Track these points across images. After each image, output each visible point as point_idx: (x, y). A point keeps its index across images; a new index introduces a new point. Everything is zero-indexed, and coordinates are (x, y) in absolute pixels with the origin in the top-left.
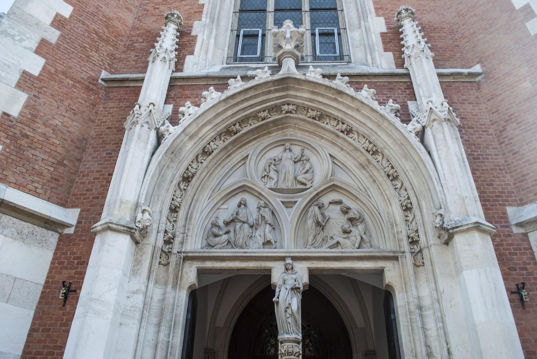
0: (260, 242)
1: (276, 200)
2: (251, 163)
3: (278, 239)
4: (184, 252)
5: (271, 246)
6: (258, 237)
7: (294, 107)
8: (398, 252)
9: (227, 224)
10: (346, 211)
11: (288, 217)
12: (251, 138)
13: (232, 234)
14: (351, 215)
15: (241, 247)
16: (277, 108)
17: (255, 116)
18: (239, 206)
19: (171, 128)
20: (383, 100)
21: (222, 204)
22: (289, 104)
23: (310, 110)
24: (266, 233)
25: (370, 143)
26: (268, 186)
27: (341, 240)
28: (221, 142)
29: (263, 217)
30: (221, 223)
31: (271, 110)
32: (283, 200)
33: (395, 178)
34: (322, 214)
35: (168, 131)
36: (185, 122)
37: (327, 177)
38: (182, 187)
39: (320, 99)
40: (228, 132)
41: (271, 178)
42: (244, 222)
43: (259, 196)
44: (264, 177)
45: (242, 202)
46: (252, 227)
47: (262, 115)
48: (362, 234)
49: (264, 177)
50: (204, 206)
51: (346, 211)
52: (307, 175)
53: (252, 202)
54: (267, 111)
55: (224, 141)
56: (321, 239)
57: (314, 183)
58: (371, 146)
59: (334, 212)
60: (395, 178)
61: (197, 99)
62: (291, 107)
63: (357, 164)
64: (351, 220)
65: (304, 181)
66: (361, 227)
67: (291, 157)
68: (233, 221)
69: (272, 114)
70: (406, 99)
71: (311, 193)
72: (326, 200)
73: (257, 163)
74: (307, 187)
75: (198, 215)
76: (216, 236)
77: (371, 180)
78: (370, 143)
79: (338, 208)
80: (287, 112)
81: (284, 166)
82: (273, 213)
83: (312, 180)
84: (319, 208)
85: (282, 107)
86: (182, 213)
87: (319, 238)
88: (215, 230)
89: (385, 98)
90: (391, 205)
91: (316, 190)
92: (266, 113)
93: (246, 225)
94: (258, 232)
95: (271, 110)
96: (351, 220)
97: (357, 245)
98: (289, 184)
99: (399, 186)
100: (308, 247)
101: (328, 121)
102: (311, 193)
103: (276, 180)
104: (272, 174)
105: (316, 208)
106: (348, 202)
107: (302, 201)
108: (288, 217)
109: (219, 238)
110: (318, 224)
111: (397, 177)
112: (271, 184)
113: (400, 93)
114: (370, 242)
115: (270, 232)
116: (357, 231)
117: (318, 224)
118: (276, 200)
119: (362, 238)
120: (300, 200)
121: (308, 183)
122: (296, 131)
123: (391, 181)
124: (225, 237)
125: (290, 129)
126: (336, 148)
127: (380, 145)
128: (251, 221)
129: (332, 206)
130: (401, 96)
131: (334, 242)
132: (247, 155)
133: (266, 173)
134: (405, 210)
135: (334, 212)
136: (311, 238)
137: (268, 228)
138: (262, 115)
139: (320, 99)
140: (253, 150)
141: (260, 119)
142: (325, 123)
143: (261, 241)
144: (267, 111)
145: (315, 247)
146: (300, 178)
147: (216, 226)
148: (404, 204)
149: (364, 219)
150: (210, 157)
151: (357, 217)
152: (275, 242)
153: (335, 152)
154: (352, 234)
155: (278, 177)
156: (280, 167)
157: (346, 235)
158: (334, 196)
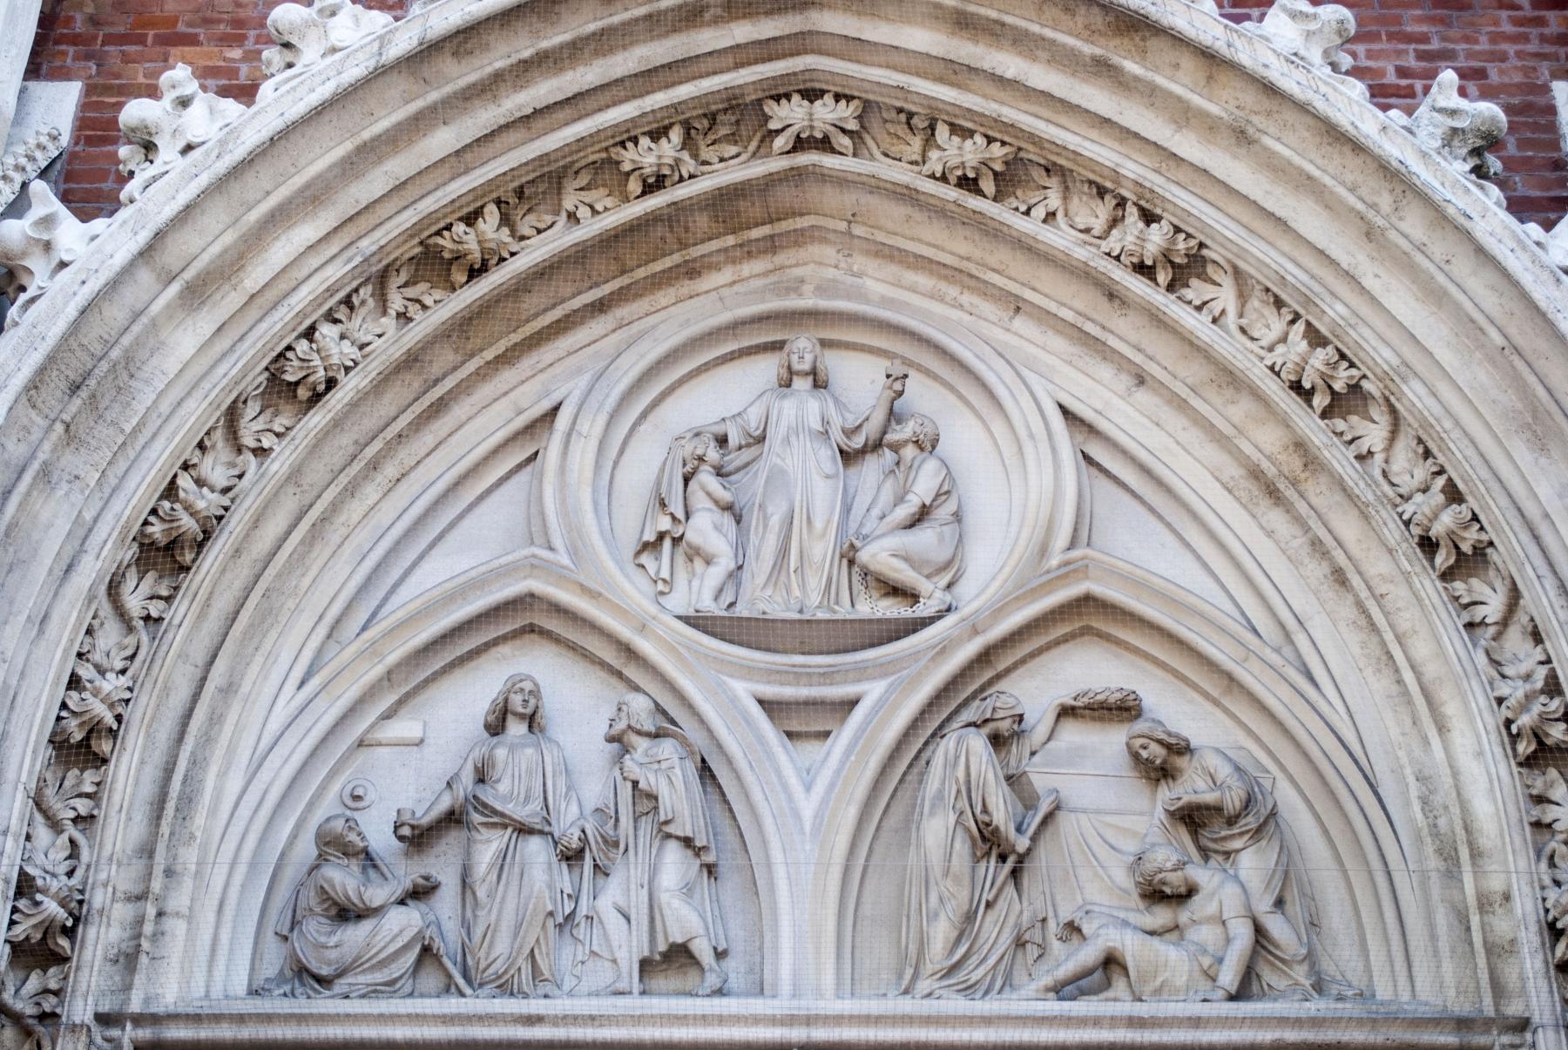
0: (621, 955)
1: (726, 694)
2: (572, 457)
3: (737, 935)
4: (138, 1020)
5: (692, 979)
6: (614, 921)
7: (847, 113)
8: (1488, 1024)
9: (418, 838)
10: (1160, 763)
11: (802, 800)
12: (577, 303)
13: (446, 903)
14: (1192, 787)
15: (506, 988)
16: (738, 117)
17: (602, 166)
18: (496, 727)
19: (71, 233)
20: (1402, 72)
21: (388, 715)
22: (812, 95)
23: (942, 132)
24: (663, 897)
25: (1316, 338)
26: (679, 601)
27: (1131, 946)
28: (389, 323)
29: (645, 798)
30: (378, 834)
31: (701, 125)
32: (771, 691)
33: (1471, 561)
34: (1014, 780)
35: (47, 246)
36: (156, 190)
37: (1043, 551)
38: (134, 603)
39: (1009, 64)
40: (433, 262)
41: (694, 553)
42: (524, 830)
43: (622, 662)
44: (652, 546)
45: (516, 701)
46: (572, 857)
47: (647, 156)
48: (1263, 905)
49: (652, 546)
50: (274, 725)
51: (1160, 763)
52: (925, 539)
53: (578, 703)
54: (676, 135)
55: (403, 317)
56: (1007, 939)
57: (966, 589)
58: (1320, 357)
59: (1087, 775)
60: (1471, 561)
61: (236, 53)
62: (826, 113)
63: (1233, 471)
64: (1192, 818)
65: (904, 574)
66: (1253, 863)
67: (825, 422)
68: (453, 819)
69: (705, 153)
70: (1544, 69)
71: (943, 649)
72: (1035, 691)
73: (609, 458)
74: (923, 610)
75: (234, 785)
76: (345, 913)
77: (1317, 570)
78: (1316, 338)
79: (1111, 741)
80: (800, 144)
81: (778, 477)
82: (705, 770)
83: (950, 569)
84: (997, 741)
85: (770, 107)
86: (130, 772)
87: (995, 932)
88: (343, 879)
89: (1411, 62)
90: (1442, 728)
91: (975, 631)
92: (669, 148)
93: (535, 845)
94: (612, 893)
95: (701, 125)
96: (1192, 818)
97: (1229, 977)
98: (811, 592)
99: (1493, 609)
100: (923, 986)
101: (1054, 201)
102: (943, 649)
103: (725, 563)
104: (706, 528)
105: (978, 743)
106: (1172, 708)
107: (887, 694)
108: (802, 800)
109: (366, 926)
110: (988, 841)
111: (1480, 553)
112: (699, 590)
113: (1508, 28)
114: (1310, 958)
115: (688, 890)
116: (1231, 889)
117: (988, 841)
118: (726, 694)
119: (1259, 930)
120: (873, 691)
121: (923, 585)
122: (860, 262)
123: (1447, 576)
124: (402, 923)
125: (815, 250)
126: (1105, 372)
127: (1378, 351)
128: (569, 822)
129: (1074, 734)
130: (1511, 49)
131: (1088, 954)
132: (546, 405)
133: (665, 523)
134: (1529, 762)
135: (1087, 775)
136: (941, 932)
137: (674, 865)
138: (647, 156)
139: (1009, 64)
140: (583, 381)
141: (634, 186)
142: (1039, 212)
143: (629, 945)
144: (676, 135)
145: (968, 990)
146: (880, 554)
147: (347, 851)
148: (1525, 720)
149: (1273, 814)
150: (317, 419)
151: (1233, 800)
152: (720, 955)
153: (1100, 393)
154: (1200, 906)
155: (740, 547)
156: (752, 486)
157: (1161, 916)
158: (1088, 670)
